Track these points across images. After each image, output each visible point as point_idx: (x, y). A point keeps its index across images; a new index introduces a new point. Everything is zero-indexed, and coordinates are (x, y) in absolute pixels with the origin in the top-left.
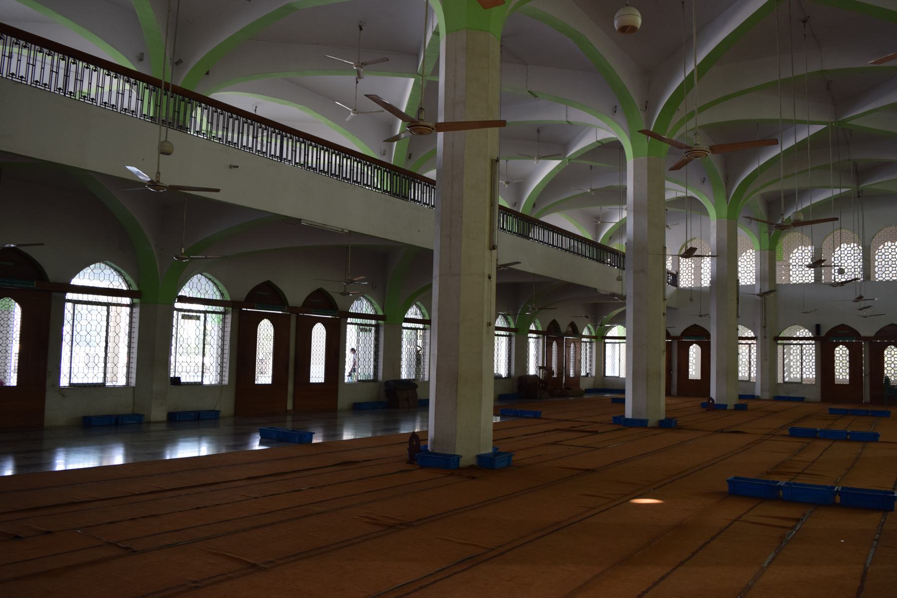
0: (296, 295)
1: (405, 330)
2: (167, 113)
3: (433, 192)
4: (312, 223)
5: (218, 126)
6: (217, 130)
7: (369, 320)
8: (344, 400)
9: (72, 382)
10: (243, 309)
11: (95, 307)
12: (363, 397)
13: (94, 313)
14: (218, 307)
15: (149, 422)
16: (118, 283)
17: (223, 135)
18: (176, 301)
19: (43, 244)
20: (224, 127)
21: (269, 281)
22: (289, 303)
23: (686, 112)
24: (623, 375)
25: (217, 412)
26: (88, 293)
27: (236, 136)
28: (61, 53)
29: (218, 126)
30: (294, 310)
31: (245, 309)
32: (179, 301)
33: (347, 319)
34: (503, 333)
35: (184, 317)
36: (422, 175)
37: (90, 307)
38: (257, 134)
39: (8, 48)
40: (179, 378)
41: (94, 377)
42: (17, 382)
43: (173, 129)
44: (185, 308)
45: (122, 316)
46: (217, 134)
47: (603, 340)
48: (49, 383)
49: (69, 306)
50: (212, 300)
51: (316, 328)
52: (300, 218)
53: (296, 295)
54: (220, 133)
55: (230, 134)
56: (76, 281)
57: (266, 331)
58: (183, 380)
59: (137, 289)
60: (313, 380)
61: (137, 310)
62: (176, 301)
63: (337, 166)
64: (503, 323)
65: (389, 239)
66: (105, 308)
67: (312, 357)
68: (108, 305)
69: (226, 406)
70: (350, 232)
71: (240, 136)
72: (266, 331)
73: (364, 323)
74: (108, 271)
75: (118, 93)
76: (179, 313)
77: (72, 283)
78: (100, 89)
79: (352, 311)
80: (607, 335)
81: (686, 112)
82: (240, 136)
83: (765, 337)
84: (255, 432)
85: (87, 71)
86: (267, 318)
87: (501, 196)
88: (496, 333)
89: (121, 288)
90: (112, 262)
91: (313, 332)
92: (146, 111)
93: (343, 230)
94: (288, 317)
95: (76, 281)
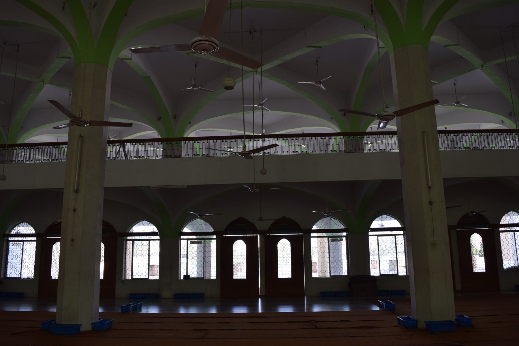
1: (11, 243)
5: (39, 154)
6: (38, 155)
9: (331, 275)
11: (140, 242)
14: (33, 238)
17: (41, 158)
18: (370, 231)
19: (222, 214)
20: (42, 154)
24: (402, 272)
25: (203, 294)
26: (15, 237)
27: (503, 142)
28: (471, 133)
31: (297, 234)
32: (371, 231)
33: (499, 229)
37: (143, 242)
38: (44, 152)
39: (146, 148)
42: (292, 276)
43: (7, 163)
44: (387, 234)
46: (38, 158)
47: (6, 238)
50: (509, 224)
54: (40, 157)
55: (37, 156)
56: (13, 232)
57: (57, 248)
59: (401, 227)
60: (280, 276)
61: (405, 236)
62: (370, 231)
66: (394, 237)
68: (149, 240)
71: (480, 143)
72: (57, 248)
74: (336, 221)
75: (498, 141)
76: (329, 238)
77: (501, 223)
78: (506, 141)
82: (480, 143)
83: (75, 210)
84: (160, 310)
85: (464, 137)
86: (476, 233)
89: (32, 233)
91: (53, 248)
92: (474, 145)
95: (502, 222)
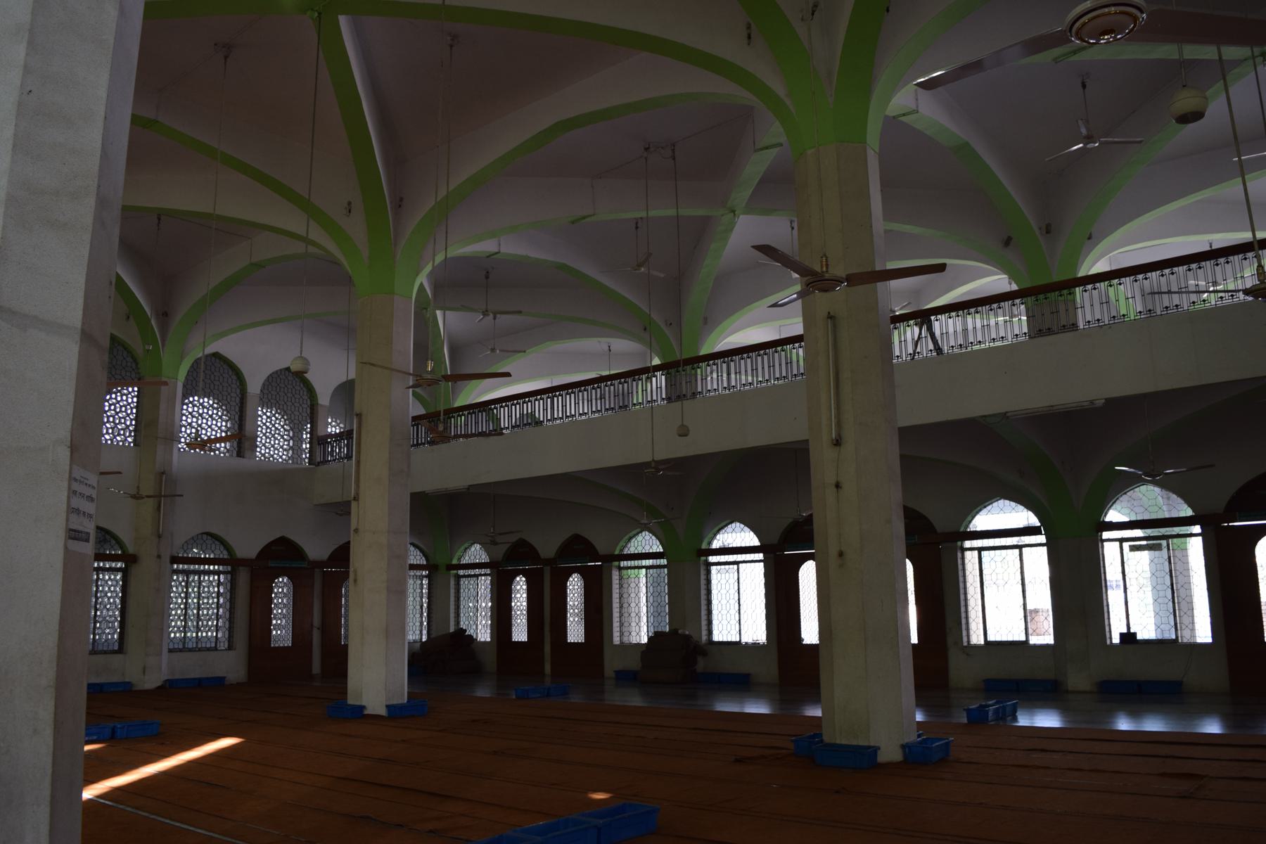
0: (548, 546)
2: (461, 420)
3: (581, 398)
4: (1029, 411)
5: (746, 371)
6: (746, 375)
7: (633, 562)
8: (611, 665)
10: (600, 563)
12: (634, 663)
13: (998, 559)
15: (1067, 692)
16: (1031, 519)
17: (753, 380)
21: (520, 539)
22: (599, 551)
23: (436, 198)
26: (741, 553)
29: (746, 371)
30: (548, 562)
34: (483, 571)
35: (1133, 549)
36: (452, 407)
40: (1135, 634)
41: (1015, 633)
44: (1111, 537)
45: (1038, 560)
46: (747, 380)
48: (950, 640)
49: (971, 557)
50: (468, 564)
51: (805, 569)
52: (1004, 411)
53: (548, 546)
54: (750, 379)
58: (1139, 637)
63: (635, 392)
64: (418, 558)
65: (783, 442)
67: (801, 605)
68: (1020, 547)
69: (768, 670)
70: (1109, 401)
73: (655, 564)
79: (464, 562)
80: (1108, 519)
81: (436, 198)
87: (454, 400)
88: (462, 574)
90: (987, 501)
93: (1092, 402)
94: (541, 571)
